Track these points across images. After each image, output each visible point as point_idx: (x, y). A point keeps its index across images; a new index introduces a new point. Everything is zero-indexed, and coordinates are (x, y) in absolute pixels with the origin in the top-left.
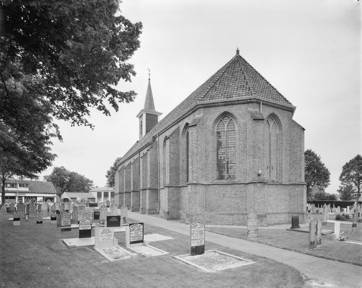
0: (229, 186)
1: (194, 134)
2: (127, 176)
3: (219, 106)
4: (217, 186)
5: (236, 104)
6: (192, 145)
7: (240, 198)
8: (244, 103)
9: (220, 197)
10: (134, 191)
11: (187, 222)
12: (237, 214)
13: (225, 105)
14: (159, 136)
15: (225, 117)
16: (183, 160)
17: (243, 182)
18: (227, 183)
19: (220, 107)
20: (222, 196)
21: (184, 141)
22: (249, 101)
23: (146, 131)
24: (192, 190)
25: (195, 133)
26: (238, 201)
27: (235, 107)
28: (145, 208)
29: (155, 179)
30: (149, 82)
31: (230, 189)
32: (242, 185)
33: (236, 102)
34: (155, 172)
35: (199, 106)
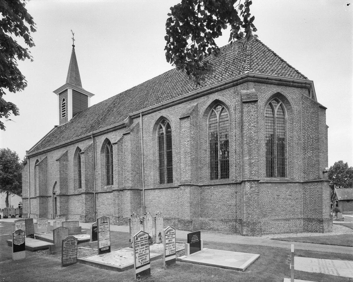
0: (284, 185)
1: (252, 113)
2: (62, 172)
3: (271, 84)
4: (270, 185)
5: (290, 86)
6: (250, 127)
7: (295, 200)
8: (298, 87)
9: (274, 198)
10: (87, 193)
11: (244, 233)
12: (293, 219)
13: (278, 85)
14: (142, 116)
15: (217, 106)
16: (206, 151)
17: (298, 181)
18: (280, 182)
19: (272, 86)
20: (276, 197)
21: (206, 125)
22: (304, 85)
23: (73, 114)
24: (253, 189)
25: (254, 111)
26: (294, 203)
27: (289, 89)
28: (122, 216)
29: (137, 176)
30: (73, 49)
31: (285, 189)
32: (297, 184)
33: (291, 83)
34: (137, 166)
35: (249, 78)
